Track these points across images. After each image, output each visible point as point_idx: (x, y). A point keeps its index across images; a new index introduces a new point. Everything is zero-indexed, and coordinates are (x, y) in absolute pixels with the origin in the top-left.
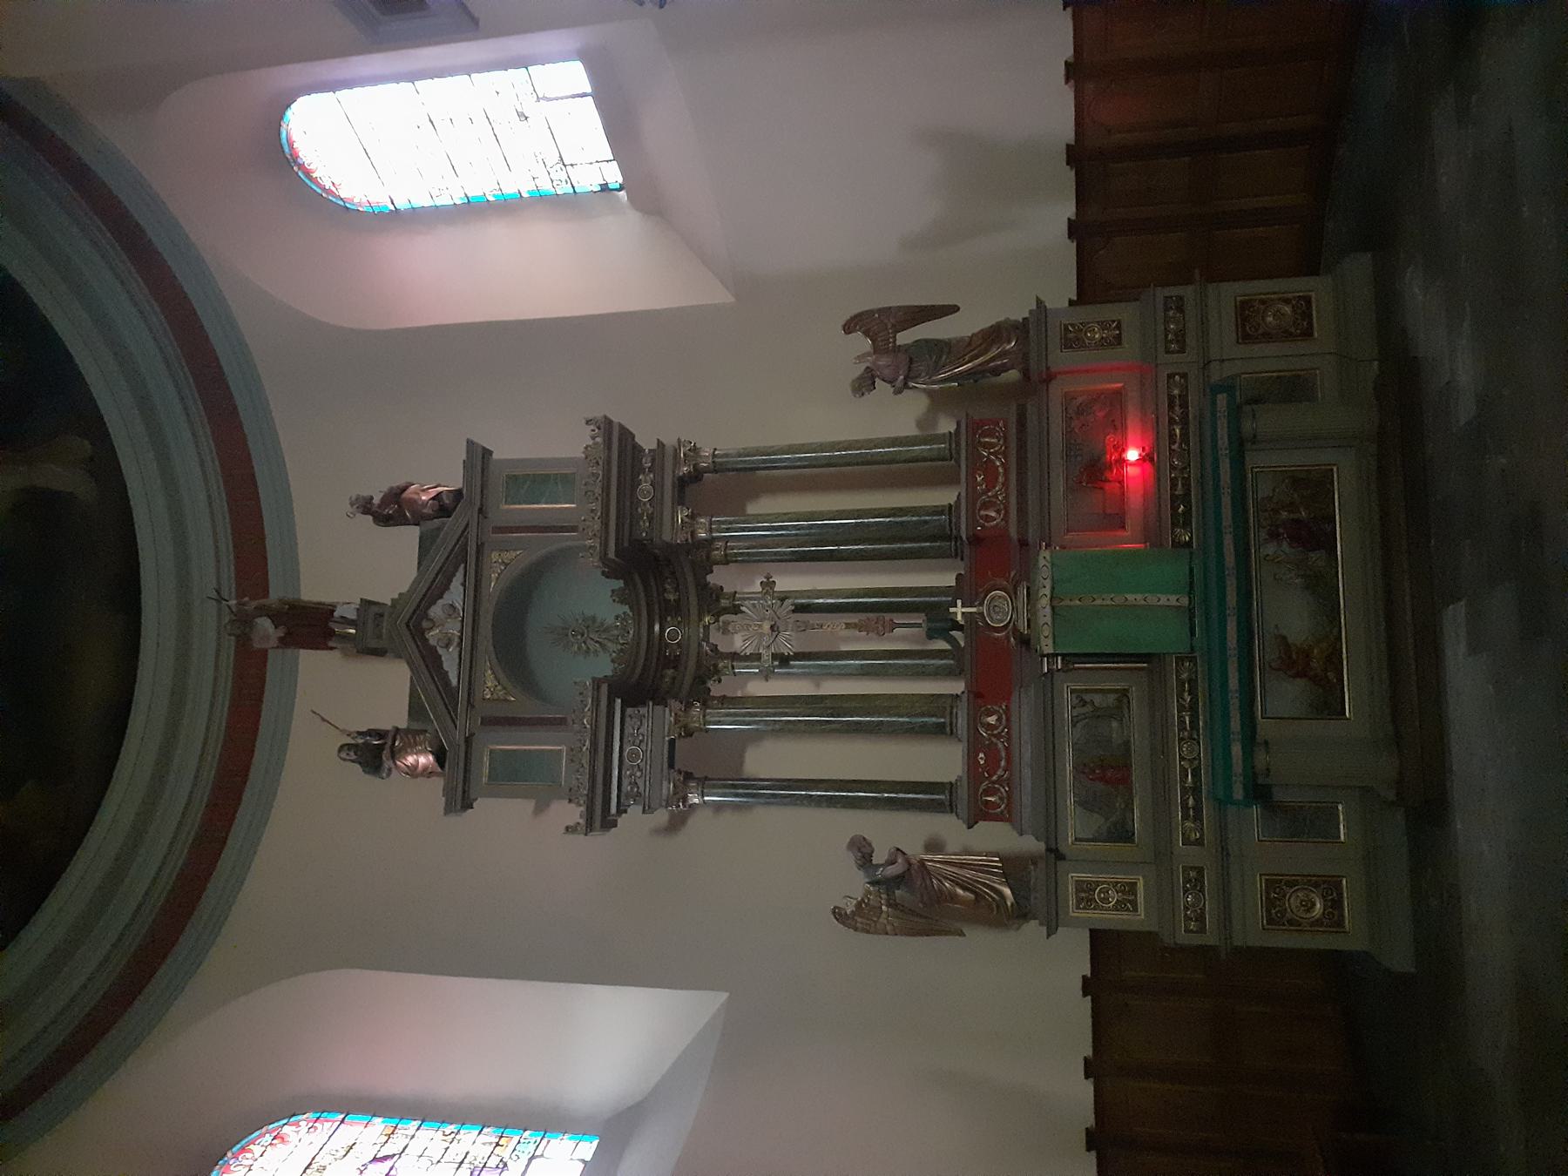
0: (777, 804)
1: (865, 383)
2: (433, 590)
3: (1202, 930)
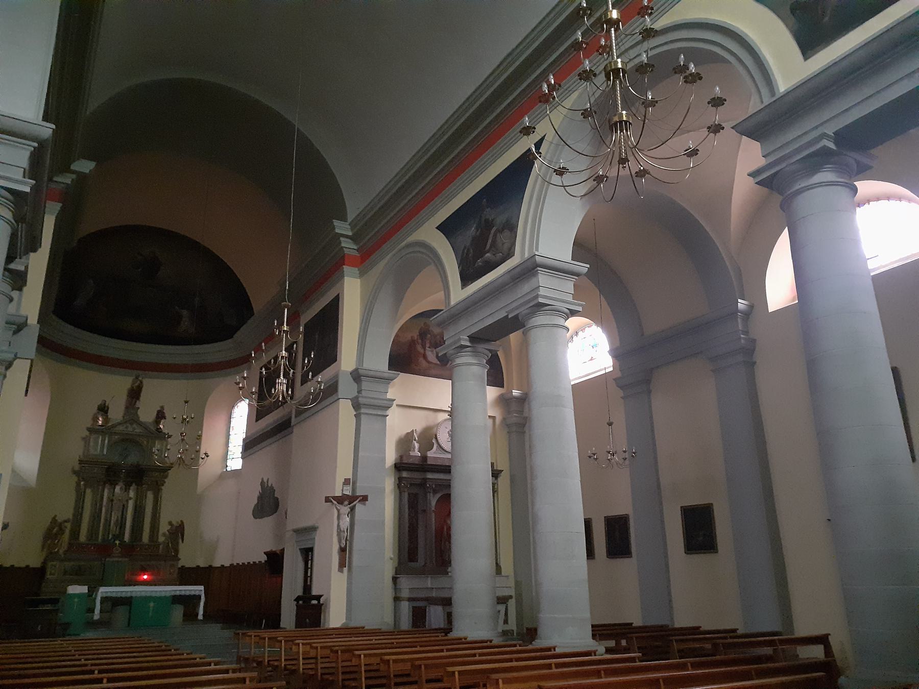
0: (18, 183)
1: (170, 523)
2: (140, 424)
3: (50, 574)
